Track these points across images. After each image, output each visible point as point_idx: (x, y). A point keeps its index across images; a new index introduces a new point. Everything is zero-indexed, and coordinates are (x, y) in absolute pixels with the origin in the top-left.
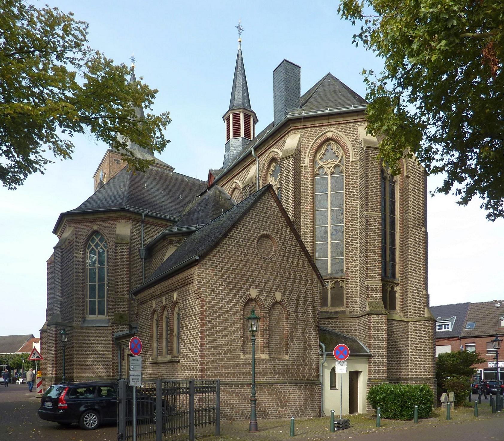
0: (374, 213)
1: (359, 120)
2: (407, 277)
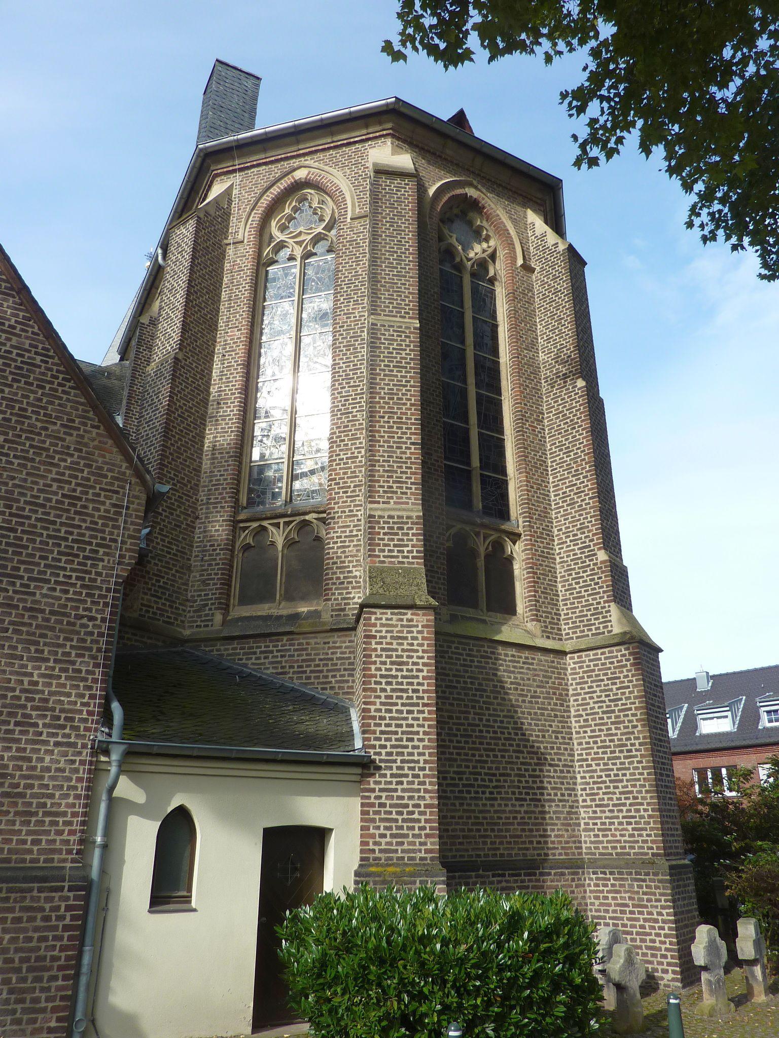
0: (398, 319)
1: (371, 136)
2: (545, 515)
